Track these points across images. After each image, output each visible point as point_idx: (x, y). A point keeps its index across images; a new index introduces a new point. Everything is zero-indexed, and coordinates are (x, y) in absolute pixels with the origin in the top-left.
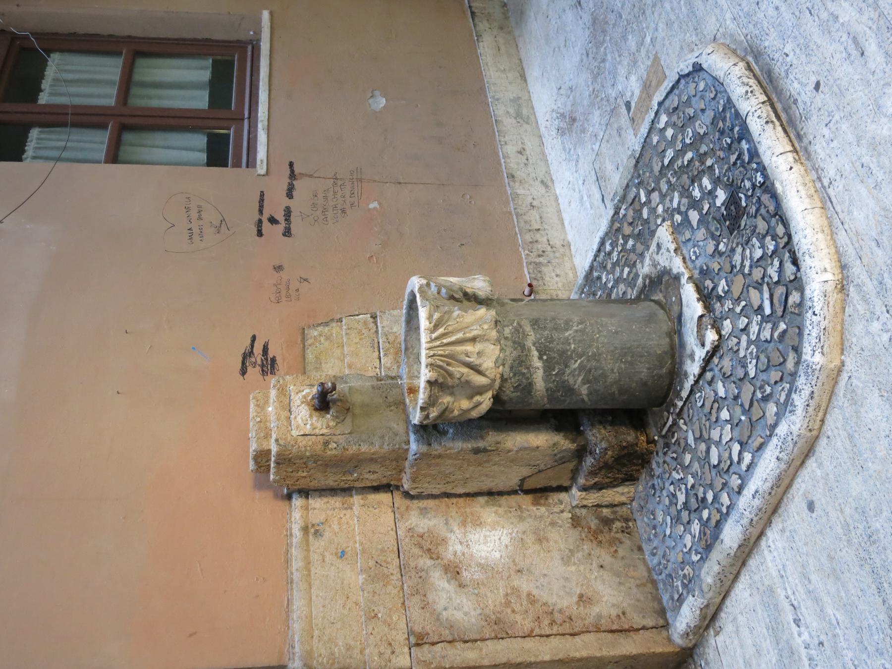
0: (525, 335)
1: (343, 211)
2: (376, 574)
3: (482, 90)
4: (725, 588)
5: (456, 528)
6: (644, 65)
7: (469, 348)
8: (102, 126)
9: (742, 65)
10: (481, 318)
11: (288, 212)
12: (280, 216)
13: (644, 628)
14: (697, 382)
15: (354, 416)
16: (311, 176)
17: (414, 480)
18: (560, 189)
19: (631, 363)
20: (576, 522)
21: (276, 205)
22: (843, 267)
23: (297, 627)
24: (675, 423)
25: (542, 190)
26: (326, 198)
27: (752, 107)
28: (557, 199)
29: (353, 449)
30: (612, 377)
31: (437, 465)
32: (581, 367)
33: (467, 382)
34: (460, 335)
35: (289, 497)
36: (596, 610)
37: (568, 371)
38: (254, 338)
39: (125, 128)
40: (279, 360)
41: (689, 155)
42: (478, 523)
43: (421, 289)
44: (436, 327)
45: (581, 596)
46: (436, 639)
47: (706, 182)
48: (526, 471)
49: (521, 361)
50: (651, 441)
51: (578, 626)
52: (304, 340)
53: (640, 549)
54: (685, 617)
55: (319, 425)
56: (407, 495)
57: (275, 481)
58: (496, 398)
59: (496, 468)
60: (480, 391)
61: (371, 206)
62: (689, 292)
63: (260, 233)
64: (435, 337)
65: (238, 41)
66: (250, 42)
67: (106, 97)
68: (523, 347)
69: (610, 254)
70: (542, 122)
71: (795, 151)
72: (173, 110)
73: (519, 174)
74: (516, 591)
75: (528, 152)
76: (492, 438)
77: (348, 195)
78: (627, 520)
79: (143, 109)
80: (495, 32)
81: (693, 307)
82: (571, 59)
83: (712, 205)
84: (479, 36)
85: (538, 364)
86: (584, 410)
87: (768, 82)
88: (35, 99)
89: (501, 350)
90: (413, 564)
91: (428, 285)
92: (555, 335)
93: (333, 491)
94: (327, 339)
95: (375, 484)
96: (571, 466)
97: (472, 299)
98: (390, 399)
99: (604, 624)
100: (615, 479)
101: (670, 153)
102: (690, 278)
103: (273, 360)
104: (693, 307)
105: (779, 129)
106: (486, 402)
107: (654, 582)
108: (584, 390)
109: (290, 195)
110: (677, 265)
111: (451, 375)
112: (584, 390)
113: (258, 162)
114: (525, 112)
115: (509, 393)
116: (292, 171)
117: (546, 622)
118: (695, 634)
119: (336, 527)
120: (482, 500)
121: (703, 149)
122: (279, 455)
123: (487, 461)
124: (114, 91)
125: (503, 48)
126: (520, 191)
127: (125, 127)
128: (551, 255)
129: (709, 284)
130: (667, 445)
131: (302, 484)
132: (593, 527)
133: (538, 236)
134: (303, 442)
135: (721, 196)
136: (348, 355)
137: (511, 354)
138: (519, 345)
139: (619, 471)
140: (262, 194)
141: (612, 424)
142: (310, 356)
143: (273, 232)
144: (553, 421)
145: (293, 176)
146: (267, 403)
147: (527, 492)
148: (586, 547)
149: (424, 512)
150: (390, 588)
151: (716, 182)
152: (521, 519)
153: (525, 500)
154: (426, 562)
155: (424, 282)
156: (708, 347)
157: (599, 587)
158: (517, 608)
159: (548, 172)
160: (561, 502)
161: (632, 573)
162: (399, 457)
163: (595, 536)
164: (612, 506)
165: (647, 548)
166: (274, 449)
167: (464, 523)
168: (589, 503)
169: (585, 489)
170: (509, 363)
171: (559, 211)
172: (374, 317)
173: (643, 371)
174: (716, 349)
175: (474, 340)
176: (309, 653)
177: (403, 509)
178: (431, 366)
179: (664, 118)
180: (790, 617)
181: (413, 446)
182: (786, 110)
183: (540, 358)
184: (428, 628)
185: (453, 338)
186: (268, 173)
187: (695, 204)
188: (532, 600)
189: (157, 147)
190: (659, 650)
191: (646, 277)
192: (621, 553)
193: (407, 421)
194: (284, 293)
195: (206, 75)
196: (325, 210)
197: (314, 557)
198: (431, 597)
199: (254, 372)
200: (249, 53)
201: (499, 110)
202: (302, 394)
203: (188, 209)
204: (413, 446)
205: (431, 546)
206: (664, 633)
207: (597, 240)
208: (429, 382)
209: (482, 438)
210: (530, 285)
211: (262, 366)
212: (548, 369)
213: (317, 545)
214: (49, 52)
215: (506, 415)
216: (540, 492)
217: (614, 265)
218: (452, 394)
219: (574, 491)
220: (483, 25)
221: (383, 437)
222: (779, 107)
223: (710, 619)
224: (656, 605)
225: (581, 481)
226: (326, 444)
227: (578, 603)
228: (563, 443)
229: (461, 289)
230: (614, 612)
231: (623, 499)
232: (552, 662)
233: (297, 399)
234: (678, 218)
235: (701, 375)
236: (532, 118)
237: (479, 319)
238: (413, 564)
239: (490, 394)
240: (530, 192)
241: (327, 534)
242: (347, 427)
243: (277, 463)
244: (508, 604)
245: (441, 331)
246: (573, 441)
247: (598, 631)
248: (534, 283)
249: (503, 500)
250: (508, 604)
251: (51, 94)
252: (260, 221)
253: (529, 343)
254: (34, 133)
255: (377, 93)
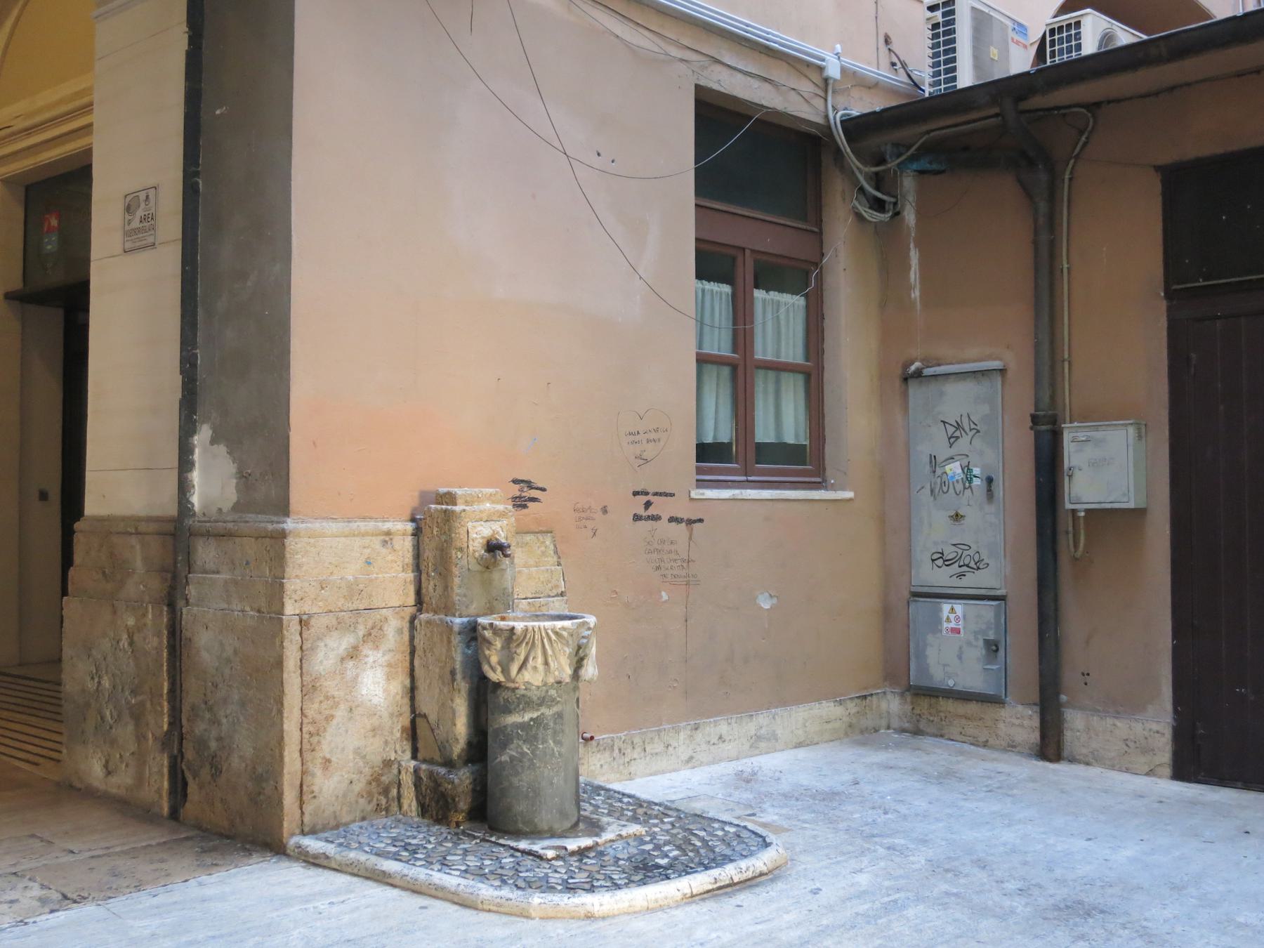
0: (549, 707)
1: (658, 568)
2: (353, 590)
3: (784, 703)
4: (344, 868)
5: (386, 658)
6: (785, 824)
7: (540, 660)
8: (735, 348)
9: (765, 869)
10: (563, 670)
11: (656, 518)
12: (651, 511)
13: (302, 813)
14: (512, 848)
15: (482, 572)
16: (690, 538)
17: (429, 622)
18: (685, 773)
19: (527, 797)
20: (387, 763)
21: (661, 507)
22: (604, 918)
23: (317, 525)
24: (475, 838)
25: (684, 757)
26: (670, 552)
27: (729, 872)
28: (675, 770)
29: (456, 571)
30: (515, 781)
31: (442, 640)
32: (523, 754)
33: (512, 659)
34: (550, 652)
35: (413, 520)
36: (318, 772)
37: (521, 743)
38: (543, 490)
39: (734, 368)
40: (525, 511)
41: (699, 844)
42: (389, 677)
43: (584, 623)
44: (556, 633)
45: (329, 761)
46: (305, 636)
47: (676, 853)
48: (433, 718)
49: (528, 703)
50: (458, 824)
51: (307, 756)
52: (541, 532)
53: (363, 819)
54: (313, 845)
55: (476, 544)
56: (413, 619)
57: (429, 509)
58: (498, 685)
59: (437, 690)
60: (505, 671)
61: (663, 594)
62: (586, 842)
63: (636, 494)
64: (551, 628)
65: (824, 469)
66: (825, 481)
67: (763, 349)
68: (540, 705)
69: (620, 801)
70: (753, 759)
71: (692, 896)
72: (753, 410)
73: (699, 736)
74: (336, 705)
75: (721, 745)
76: (463, 686)
77: (675, 572)
78: (387, 810)
79: (753, 386)
80: (846, 719)
81: (573, 844)
82: (805, 779)
83: (657, 857)
84: (840, 703)
85: (527, 717)
86: (486, 767)
87: (748, 883)
88: (757, 287)
89: (538, 687)
90: (360, 620)
91: (589, 629)
92: (549, 732)
93: (417, 555)
94: (543, 553)
95: (424, 591)
96: (437, 757)
97: (579, 663)
98: (495, 603)
99: (308, 779)
100: (424, 797)
101: (702, 834)
102: (597, 844)
103: (525, 507)
104: (573, 844)
105: (710, 887)
106: (496, 676)
107: (337, 827)
108: (505, 758)
109: (672, 520)
110: (608, 836)
111: (519, 645)
112: (505, 758)
113: (701, 491)
114: (763, 745)
115: (504, 695)
116: (695, 522)
117: (312, 729)
118: (300, 853)
119: (390, 558)
120: (408, 682)
121: (702, 851)
122: (453, 512)
123: (443, 683)
124: (770, 357)
125: (829, 726)
126: (682, 735)
127: (736, 369)
128: (621, 761)
129: (592, 854)
130: (456, 834)
131: (426, 530)
132: (383, 778)
133: (638, 750)
134: (463, 531)
135: (663, 862)
136: (529, 570)
137: (534, 695)
138: (542, 702)
139: (431, 799)
140: (672, 495)
141: (474, 790)
142: (528, 538)
143: (638, 506)
144: (475, 741)
145: (690, 522)
146: (493, 502)
147: (413, 722)
148: (367, 770)
149: (400, 631)
150: (342, 601)
151: (676, 858)
152: (392, 715)
153: (406, 720)
154: (361, 631)
155: (592, 625)
156: (541, 852)
157: (336, 778)
158: (324, 706)
159: (701, 764)
160: (403, 752)
161: (345, 809)
162: (448, 609)
163: (376, 779)
164: (399, 797)
165: (365, 824)
166: (457, 508)
167: (389, 665)
168: (403, 776)
169: (416, 771)
170: (529, 694)
171: (663, 772)
172: (562, 594)
173: (521, 807)
174: (540, 857)
175: (546, 663)
176: (298, 535)
177: (402, 614)
178: (526, 630)
179: (732, 830)
180: (334, 900)
181: (458, 620)
182: (726, 894)
183: (532, 719)
184: (312, 630)
185: (547, 646)
186: (692, 499)
187: (658, 847)
188: (329, 718)
189: (717, 398)
190: (285, 824)
191: (599, 820)
192: (362, 801)
193: (479, 616)
194: (583, 515)
195: (790, 439)
196: (659, 551)
197: (367, 540)
198: (335, 634)
199: (515, 490)
200: (813, 479)
201: (762, 719)
202: (500, 530)
203: (656, 430)
204: (458, 620)
205: (373, 636)
206: (297, 831)
207: (633, 792)
208: (513, 628)
209: (464, 678)
210: (592, 738)
211: (520, 497)
212: (524, 726)
213: (376, 542)
214: (806, 296)
215: (484, 695)
216: (413, 733)
217: (611, 805)
218: (503, 648)
219: (413, 763)
220: (852, 707)
221: (465, 596)
222: (729, 890)
223: (315, 861)
224: (319, 827)
225: (424, 767)
226: (461, 549)
227: (324, 758)
228: (458, 748)
229: (586, 656)
230: (316, 788)
231: (405, 807)
232: (282, 731)
233: (496, 526)
234: (648, 839)
235: (518, 850)
236: (757, 752)
237: (564, 670)
238: (360, 620)
239: (502, 679)
240: (681, 742)
241: (384, 551)
242: (474, 567)
243: (446, 511)
244: (327, 698)
245: (553, 637)
246: (459, 756)
247: (303, 773)
248: (593, 742)
249: (407, 701)
250: (327, 698)
251: (764, 301)
252: (647, 494)
253: (543, 710)
254: (726, 289)
255: (775, 601)
